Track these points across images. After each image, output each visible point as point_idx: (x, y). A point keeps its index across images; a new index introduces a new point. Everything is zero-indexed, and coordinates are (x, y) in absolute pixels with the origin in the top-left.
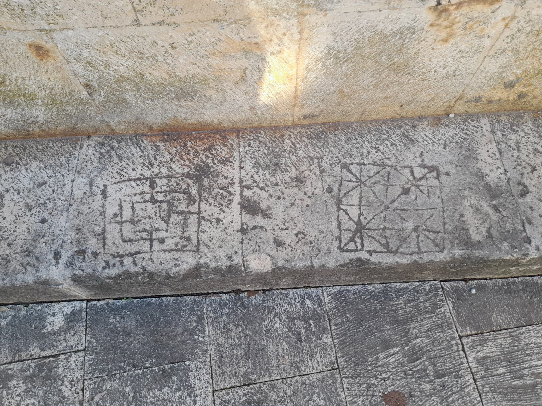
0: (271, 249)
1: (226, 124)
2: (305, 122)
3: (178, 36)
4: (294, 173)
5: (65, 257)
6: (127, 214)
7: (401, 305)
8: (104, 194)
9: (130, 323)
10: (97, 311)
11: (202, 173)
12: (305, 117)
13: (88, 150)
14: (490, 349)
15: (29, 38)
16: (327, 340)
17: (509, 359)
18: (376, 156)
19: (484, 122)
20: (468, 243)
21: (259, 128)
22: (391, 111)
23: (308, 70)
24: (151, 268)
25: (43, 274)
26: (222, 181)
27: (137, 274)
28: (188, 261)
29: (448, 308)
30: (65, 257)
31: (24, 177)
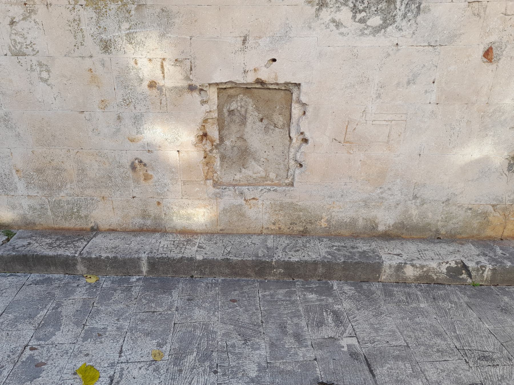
0: (204, 255)
1: (198, 231)
2: (221, 232)
3: (190, 202)
4: (215, 242)
5: (147, 253)
6: (166, 246)
7: (243, 283)
8: (160, 243)
9: (156, 281)
10: (147, 278)
11: (188, 241)
12: (221, 230)
13: (158, 235)
14: (267, 293)
15: (157, 200)
16: (217, 288)
17: (272, 295)
18: (239, 240)
19: (272, 236)
20: (258, 257)
21: (207, 233)
22: (245, 231)
23: (220, 214)
24: (169, 256)
25: (140, 255)
26: (194, 242)
27: (165, 258)
28: (180, 255)
29: (257, 284)
30: (147, 253)
31: (138, 239)
